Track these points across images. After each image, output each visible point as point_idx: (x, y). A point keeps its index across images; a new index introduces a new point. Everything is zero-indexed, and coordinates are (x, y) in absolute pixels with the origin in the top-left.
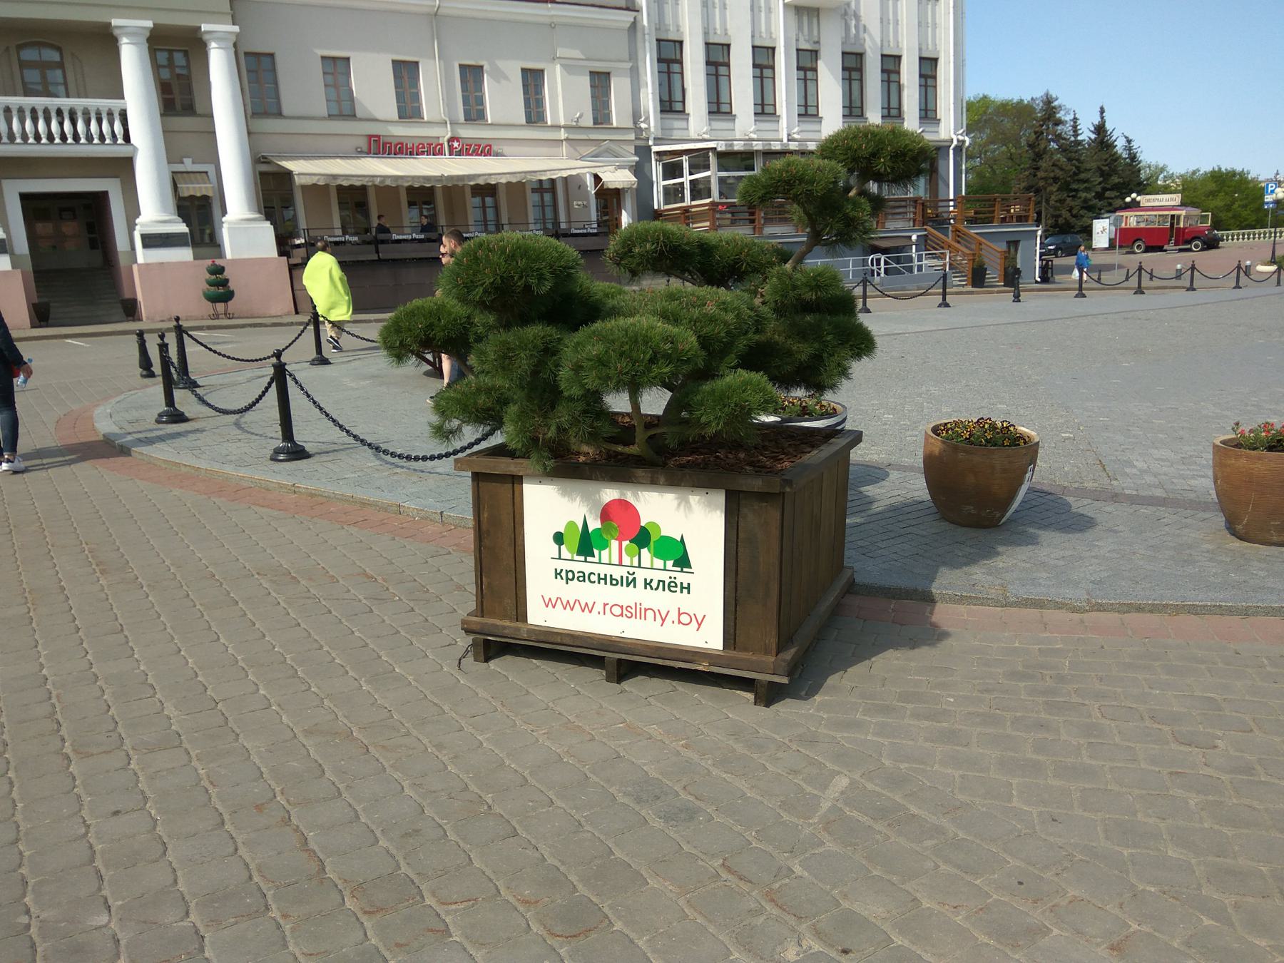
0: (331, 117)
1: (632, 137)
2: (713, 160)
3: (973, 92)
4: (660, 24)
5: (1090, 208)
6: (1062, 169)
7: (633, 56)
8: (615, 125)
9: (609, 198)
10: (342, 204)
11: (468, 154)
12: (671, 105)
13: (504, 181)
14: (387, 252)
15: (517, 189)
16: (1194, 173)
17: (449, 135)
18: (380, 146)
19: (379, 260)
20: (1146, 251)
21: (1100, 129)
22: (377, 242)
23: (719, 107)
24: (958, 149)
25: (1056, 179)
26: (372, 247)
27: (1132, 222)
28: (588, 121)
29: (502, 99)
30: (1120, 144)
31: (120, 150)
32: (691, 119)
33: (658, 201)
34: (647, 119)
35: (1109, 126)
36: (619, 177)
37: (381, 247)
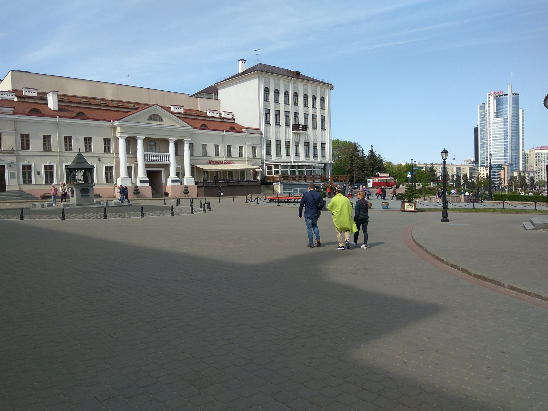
0: (203, 156)
3: (333, 138)
4: (266, 137)
5: (367, 176)
7: (261, 143)
9: (255, 174)
12: (268, 153)
15: (236, 171)
18: (211, 162)
21: (371, 151)
24: (330, 164)
25: (357, 167)
27: (377, 181)
29: (235, 152)
30: (377, 156)
31: (167, 163)
33: (265, 174)
35: (374, 151)
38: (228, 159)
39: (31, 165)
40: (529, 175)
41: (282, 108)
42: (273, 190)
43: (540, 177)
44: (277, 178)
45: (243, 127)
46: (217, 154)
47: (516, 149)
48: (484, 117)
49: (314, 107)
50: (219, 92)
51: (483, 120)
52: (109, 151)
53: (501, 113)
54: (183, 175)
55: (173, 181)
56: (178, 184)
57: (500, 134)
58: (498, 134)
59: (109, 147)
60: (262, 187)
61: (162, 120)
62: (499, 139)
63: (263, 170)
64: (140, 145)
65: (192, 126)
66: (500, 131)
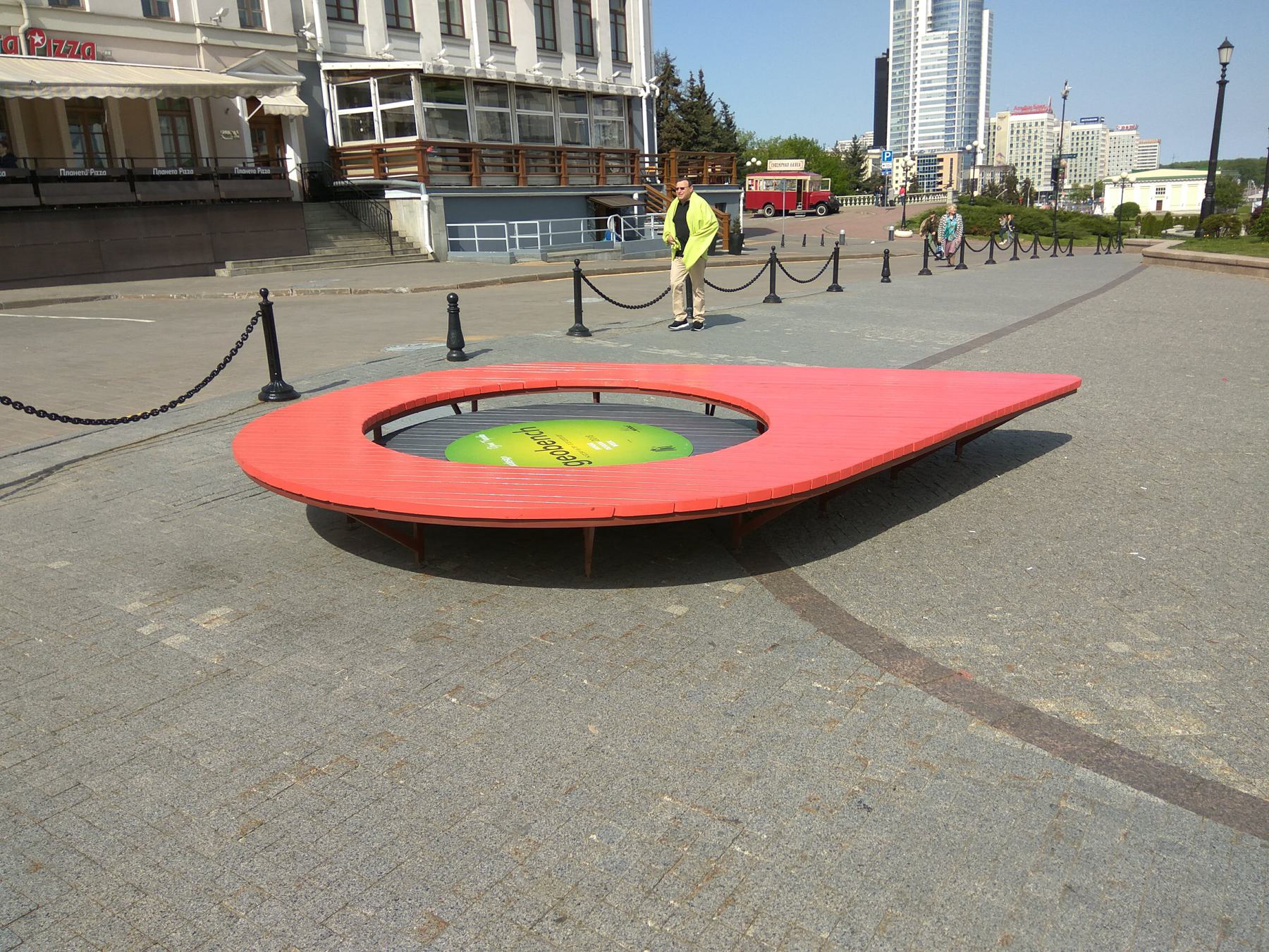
1: (294, 48)
2: (414, 83)
6: (682, 131)
8: (269, 30)
9: (270, 130)
11: (58, 55)
13: (118, 94)
14: (53, 194)
15: (132, 108)
16: (776, 140)
17: (26, 24)
19: (42, 206)
20: (775, 215)
22: (34, 179)
25: (678, 139)
26: (29, 188)
27: (762, 187)
28: (233, 22)
30: (718, 108)
32: (367, 32)
33: (333, 135)
34: (313, 25)
35: (708, 91)
36: (286, 102)
37: (43, 187)
38: (56, 23)
42: (386, 232)
44: (400, 159)
47: (973, 115)
48: (903, 30)
51: (901, 38)
53: (944, 20)
57: (938, 73)
58: (934, 74)
60: (314, 212)
62: (937, 88)
63: (318, 113)
66: (939, 66)
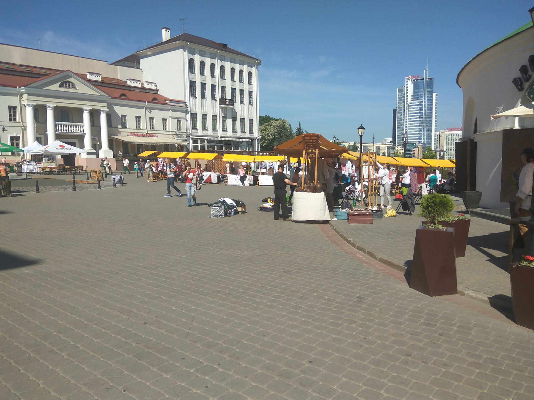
10: (437, 157)
12: (194, 126)
18: (132, 134)
21: (299, 129)
23: (205, 128)
35: (302, 129)
39: (19, 137)
40: (440, 154)
41: (209, 81)
43: (450, 156)
45: (166, 99)
46: (138, 126)
49: (241, 81)
50: (141, 61)
52: (15, 120)
54: (100, 147)
55: (88, 154)
56: (95, 157)
59: (15, 116)
61: (75, 88)
64: (50, 113)
65: (109, 96)
